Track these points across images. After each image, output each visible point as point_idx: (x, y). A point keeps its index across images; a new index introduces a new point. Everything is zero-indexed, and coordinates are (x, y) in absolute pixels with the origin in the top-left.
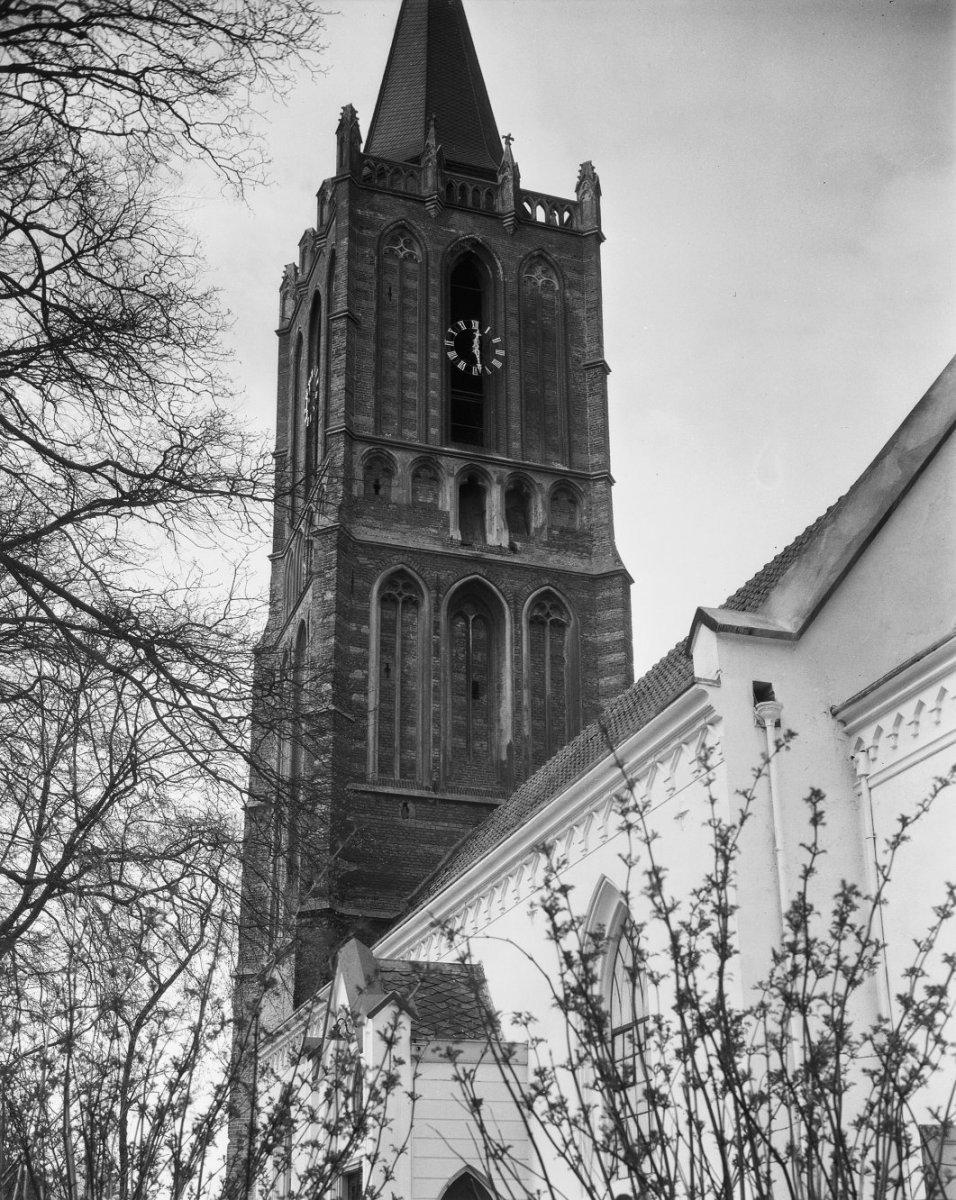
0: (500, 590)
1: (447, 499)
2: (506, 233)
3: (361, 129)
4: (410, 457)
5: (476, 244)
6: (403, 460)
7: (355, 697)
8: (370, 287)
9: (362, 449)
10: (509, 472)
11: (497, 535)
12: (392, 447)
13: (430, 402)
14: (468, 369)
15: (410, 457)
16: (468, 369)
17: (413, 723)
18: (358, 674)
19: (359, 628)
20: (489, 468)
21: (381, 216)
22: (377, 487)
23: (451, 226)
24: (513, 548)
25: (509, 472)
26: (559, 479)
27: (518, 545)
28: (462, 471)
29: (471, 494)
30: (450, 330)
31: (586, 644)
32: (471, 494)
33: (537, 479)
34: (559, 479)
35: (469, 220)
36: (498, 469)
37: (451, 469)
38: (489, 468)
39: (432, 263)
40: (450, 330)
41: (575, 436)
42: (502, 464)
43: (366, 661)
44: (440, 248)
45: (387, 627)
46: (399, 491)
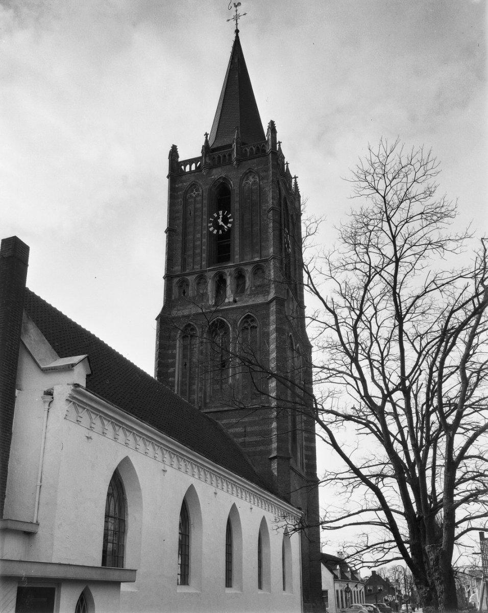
0: (240, 318)
1: (210, 287)
2: (235, 168)
3: (264, 131)
4: (194, 277)
5: (224, 179)
6: (191, 279)
7: (170, 379)
8: (180, 215)
9: (176, 280)
10: (233, 269)
11: (230, 298)
12: (186, 276)
13: (203, 251)
14: (223, 231)
15: (194, 277)
16: (223, 231)
17: (194, 384)
18: (171, 370)
19: (172, 352)
20: (226, 271)
21: (185, 184)
22: (184, 293)
23: (212, 176)
24: (235, 301)
25: (233, 269)
26: (196, 275)
27: (237, 299)
28: (215, 276)
29: (221, 283)
30: (211, 219)
31: (265, 333)
32: (221, 283)
33: (245, 268)
34: (196, 275)
35: (220, 170)
36: (229, 270)
37: (210, 275)
38: (226, 271)
39: (204, 194)
40: (211, 219)
41: (263, 244)
42: (231, 267)
43: (175, 364)
44: (207, 187)
45: (185, 348)
46: (191, 292)
